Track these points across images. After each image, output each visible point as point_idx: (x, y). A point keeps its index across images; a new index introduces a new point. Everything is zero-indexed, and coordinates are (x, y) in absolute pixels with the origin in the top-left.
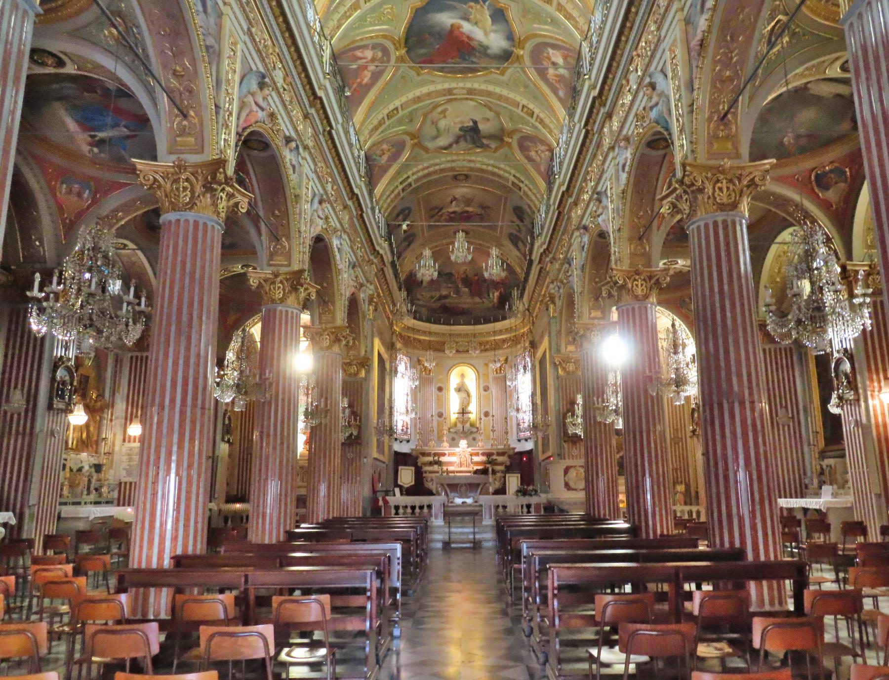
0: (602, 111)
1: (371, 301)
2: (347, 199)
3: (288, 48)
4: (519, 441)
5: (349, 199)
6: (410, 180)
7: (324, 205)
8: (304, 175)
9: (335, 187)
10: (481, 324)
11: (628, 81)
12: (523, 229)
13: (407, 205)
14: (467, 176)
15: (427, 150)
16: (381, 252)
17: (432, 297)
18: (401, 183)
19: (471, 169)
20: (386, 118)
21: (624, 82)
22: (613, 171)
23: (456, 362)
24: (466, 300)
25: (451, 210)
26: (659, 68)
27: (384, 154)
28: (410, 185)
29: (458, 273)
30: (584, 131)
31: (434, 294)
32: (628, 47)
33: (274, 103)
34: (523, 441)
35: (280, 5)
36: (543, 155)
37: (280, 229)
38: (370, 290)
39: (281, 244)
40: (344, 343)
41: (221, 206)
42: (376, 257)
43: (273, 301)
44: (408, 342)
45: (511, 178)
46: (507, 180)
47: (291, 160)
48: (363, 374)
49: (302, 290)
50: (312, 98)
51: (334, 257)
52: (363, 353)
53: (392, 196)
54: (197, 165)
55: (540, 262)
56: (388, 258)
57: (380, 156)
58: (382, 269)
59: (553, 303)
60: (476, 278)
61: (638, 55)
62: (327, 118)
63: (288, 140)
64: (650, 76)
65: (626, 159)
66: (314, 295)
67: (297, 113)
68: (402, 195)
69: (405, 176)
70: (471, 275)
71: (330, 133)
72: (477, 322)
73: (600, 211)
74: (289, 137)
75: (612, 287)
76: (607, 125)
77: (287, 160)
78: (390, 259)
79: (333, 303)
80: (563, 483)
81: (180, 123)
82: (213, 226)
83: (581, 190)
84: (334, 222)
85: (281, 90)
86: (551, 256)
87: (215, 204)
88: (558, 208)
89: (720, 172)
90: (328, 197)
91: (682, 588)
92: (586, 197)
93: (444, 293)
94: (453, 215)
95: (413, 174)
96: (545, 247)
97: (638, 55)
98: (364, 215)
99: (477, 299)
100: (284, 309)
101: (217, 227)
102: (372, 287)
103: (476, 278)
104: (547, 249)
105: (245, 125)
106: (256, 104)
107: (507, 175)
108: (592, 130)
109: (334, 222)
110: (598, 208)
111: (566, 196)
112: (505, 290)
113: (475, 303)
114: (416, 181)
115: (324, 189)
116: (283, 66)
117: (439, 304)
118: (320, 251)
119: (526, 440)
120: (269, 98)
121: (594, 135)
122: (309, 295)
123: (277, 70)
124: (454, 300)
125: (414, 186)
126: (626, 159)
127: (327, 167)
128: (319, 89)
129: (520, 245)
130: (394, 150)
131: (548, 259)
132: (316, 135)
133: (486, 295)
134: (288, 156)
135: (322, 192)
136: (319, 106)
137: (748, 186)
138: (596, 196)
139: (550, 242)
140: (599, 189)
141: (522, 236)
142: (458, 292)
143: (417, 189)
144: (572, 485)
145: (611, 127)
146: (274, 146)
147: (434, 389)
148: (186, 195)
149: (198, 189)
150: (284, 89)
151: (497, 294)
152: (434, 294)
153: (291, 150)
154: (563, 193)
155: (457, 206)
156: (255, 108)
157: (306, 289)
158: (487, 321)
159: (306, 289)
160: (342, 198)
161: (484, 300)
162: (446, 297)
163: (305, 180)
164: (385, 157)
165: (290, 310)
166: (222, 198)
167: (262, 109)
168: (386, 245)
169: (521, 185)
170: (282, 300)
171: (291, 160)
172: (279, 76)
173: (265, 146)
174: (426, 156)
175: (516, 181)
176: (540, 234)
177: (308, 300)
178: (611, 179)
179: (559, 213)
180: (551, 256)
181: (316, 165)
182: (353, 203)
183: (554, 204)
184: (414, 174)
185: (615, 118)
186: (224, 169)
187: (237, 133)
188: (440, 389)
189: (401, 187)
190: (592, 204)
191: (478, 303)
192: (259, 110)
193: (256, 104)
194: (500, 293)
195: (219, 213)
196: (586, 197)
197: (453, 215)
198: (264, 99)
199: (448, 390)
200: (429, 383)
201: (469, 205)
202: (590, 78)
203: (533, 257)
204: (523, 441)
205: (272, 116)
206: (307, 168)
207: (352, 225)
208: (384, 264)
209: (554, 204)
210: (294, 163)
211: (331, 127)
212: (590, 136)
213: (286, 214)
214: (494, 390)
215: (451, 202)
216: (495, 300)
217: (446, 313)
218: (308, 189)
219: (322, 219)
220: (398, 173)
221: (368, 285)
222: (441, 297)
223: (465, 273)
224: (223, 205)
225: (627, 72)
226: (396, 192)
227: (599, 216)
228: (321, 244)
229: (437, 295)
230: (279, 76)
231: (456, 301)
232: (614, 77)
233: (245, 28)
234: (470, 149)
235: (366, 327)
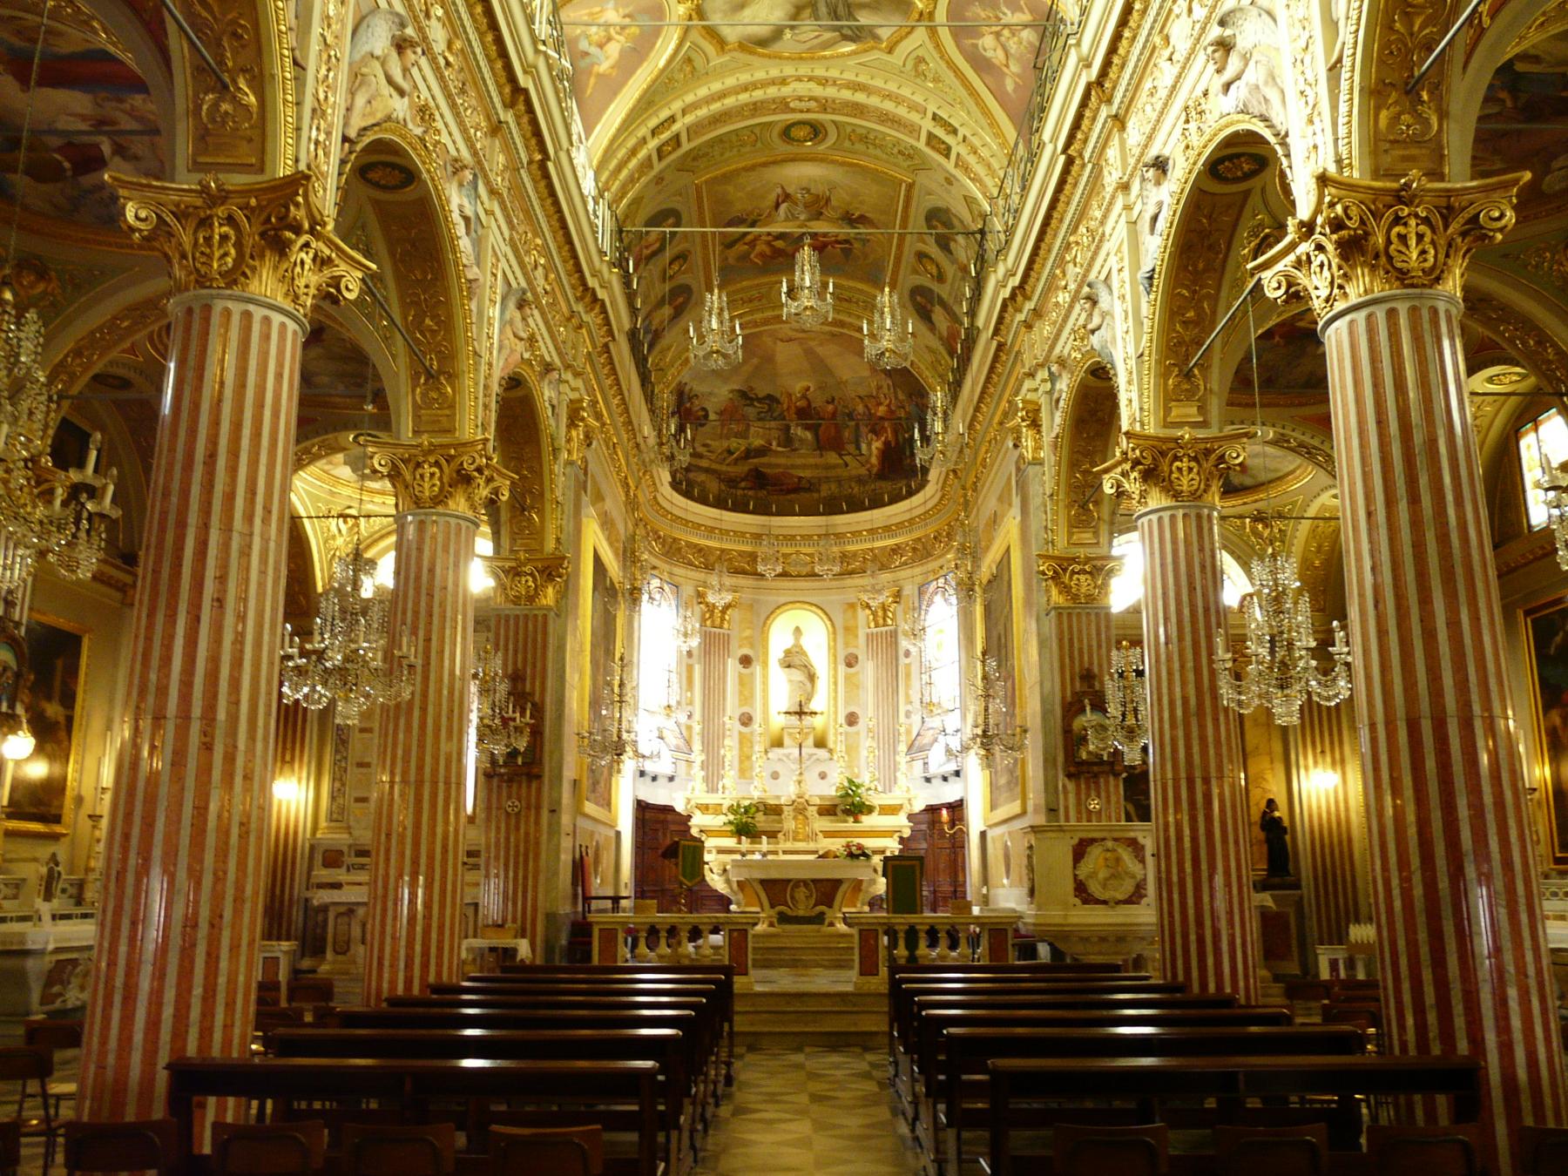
0: (1104, 112)
1: (574, 418)
2: (499, 105)
3: (481, 35)
4: (928, 780)
5: (505, 106)
6: (675, 128)
7: (410, 56)
8: (486, 247)
9: (458, 45)
10: (842, 513)
11: (1167, 39)
12: (950, 270)
13: (678, 207)
14: (817, 131)
15: (722, 44)
16: (601, 294)
17: (730, 452)
18: (654, 132)
19: (825, 105)
20: (655, 157)
21: (1157, 40)
22: (1124, 234)
23: (782, 600)
24: (804, 462)
25: (776, 229)
26: (1102, 277)
27: (609, 39)
28: (676, 138)
29: (790, 395)
30: (1062, 158)
31: (734, 443)
32: (1147, 26)
33: (428, 87)
34: (937, 782)
35: (489, 13)
36: (1013, 46)
37: (438, 363)
38: (573, 389)
39: (235, 100)
40: (484, 492)
41: (301, 282)
42: (589, 310)
43: (202, 281)
44: (673, 551)
45: (928, 125)
46: (913, 130)
47: (461, 207)
48: (549, 596)
49: (482, 482)
50: (507, 90)
51: (453, 239)
52: (550, 545)
53: (634, 163)
54: (246, 192)
55: (996, 332)
56: (621, 319)
57: (601, 46)
58: (606, 345)
59: (1035, 424)
60: (830, 407)
61: (1077, 243)
62: (537, 133)
63: (457, 167)
64: (1089, 285)
65: (1160, 204)
66: (507, 494)
67: (474, 119)
68: (658, 166)
69: (664, 114)
70: (818, 402)
71: (543, 166)
72: (832, 508)
73: (1096, 321)
74: (548, 364)
75: (1125, 474)
76: (1115, 141)
77: (454, 206)
78: (627, 326)
79: (452, 377)
80: (1070, 885)
81: (215, 105)
82: (283, 325)
83: (1050, 287)
84: (547, 350)
85: (442, 62)
86: (1029, 305)
87: (289, 280)
88: (1064, 151)
89: (1400, 200)
90: (535, 294)
91: (1211, 1110)
92: (1063, 298)
93: (758, 442)
94: (779, 244)
95: (684, 112)
96: (1016, 281)
97: (1077, 243)
98: (550, 165)
99: (832, 458)
100: (236, 308)
101: (292, 326)
102: (579, 383)
103: (830, 407)
104: (1022, 286)
105: (364, 124)
106: (390, 81)
107: (914, 117)
108: (1081, 155)
109: (547, 350)
110: (1090, 315)
111: (1010, 309)
112: (895, 433)
113: (828, 467)
114: (692, 130)
115: (529, 282)
116: (446, 12)
117: (742, 469)
118: (517, 414)
119: (945, 779)
120: (415, 71)
121: (1083, 166)
122: (496, 491)
123: (434, 22)
124: (778, 461)
125: (686, 146)
126: (1160, 204)
127: (536, 235)
128: (525, 72)
129: (938, 315)
130: (634, 30)
131: (1021, 317)
132: (513, 167)
133: (851, 448)
134: (456, 200)
135: (524, 284)
136: (521, 107)
137: (1464, 234)
138: (1086, 289)
139: (1107, 63)
140: (1092, 277)
141: (943, 291)
142: (787, 441)
143: (695, 156)
144: (1095, 888)
145: (1123, 143)
146: (425, 175)
147: (732, 665)
148: (226, 254)
149: (252, 239)
150: (448, 64)
151: (877, 445)
152: (734, 443)
153: (461, 185)
154: (1005, 300)
155: (791, 217)
156: (386, 90)
157: (489, 480)
158: (856, 506)
159: (489, 480)
160: (485, 96)
161: (848, 458)
162: (762, 452)
163: (490, 259)
164: (613, 50)
165: (258, 313)
166: (302, 263)
167: (402, 93)
168: (613, 277)
169: (949, 140)
170: (235, 277)
171: (461, 207)
172: (438, 34)
173: (409, 175)
174: (717, 60)
175: (940, 132)
176: (1002, 250)
177: (334, 300)
178: (1119, 250)
179: (1070, 162)
180: (1029, 305)
181: (512, 227)
182: (518, 117)
183: (1054, 138)
184: (690, 106)
185: (1132, 123)
186: (306, 197)
187: (345, 139)
188: (746, 661)
189: (653, 144)
190: (1077, 308)
191: (835, 466)
192: (394, 94)
193: (390, 81)
194: (887, 443)
195: (297, 297)
196: (1063, 298)
197: (779, 244)
198: (406, 71)
199: (765, 664)
200: (720, 644)
201: (818, 216)
202: (1078, 44)
203: (980, 323)
204: (937, 782)
205: (425, 114)
206: (497, 235)
207: (517, 188)
208: (610, 333)
209: (1054, 138)
210: (469, 212)
211: (546, 157)
212: (1075, 169)
213: (447, 325)
214: (868, 670)
215: (777, 206)
216: (874, 460)
217: (758, 488)
218: (494, 275)
219: (521, 339)
220: (647, 103)
221: (568, 376)
222: (749, 454)
223: (804, 396)
224: (310, 279)
225: (1061, 262)
226: (642, 154)
227: (1093, 332)
228: (518, 393)
229: (738, 445)
230: (438, 34)
231: (782, 461)
232: (1134, 37)
233: (507, 236)
234: (826, 45)
235: (560, 480)
